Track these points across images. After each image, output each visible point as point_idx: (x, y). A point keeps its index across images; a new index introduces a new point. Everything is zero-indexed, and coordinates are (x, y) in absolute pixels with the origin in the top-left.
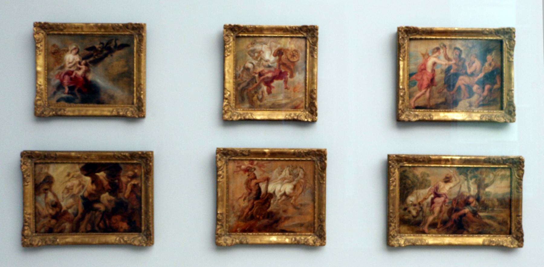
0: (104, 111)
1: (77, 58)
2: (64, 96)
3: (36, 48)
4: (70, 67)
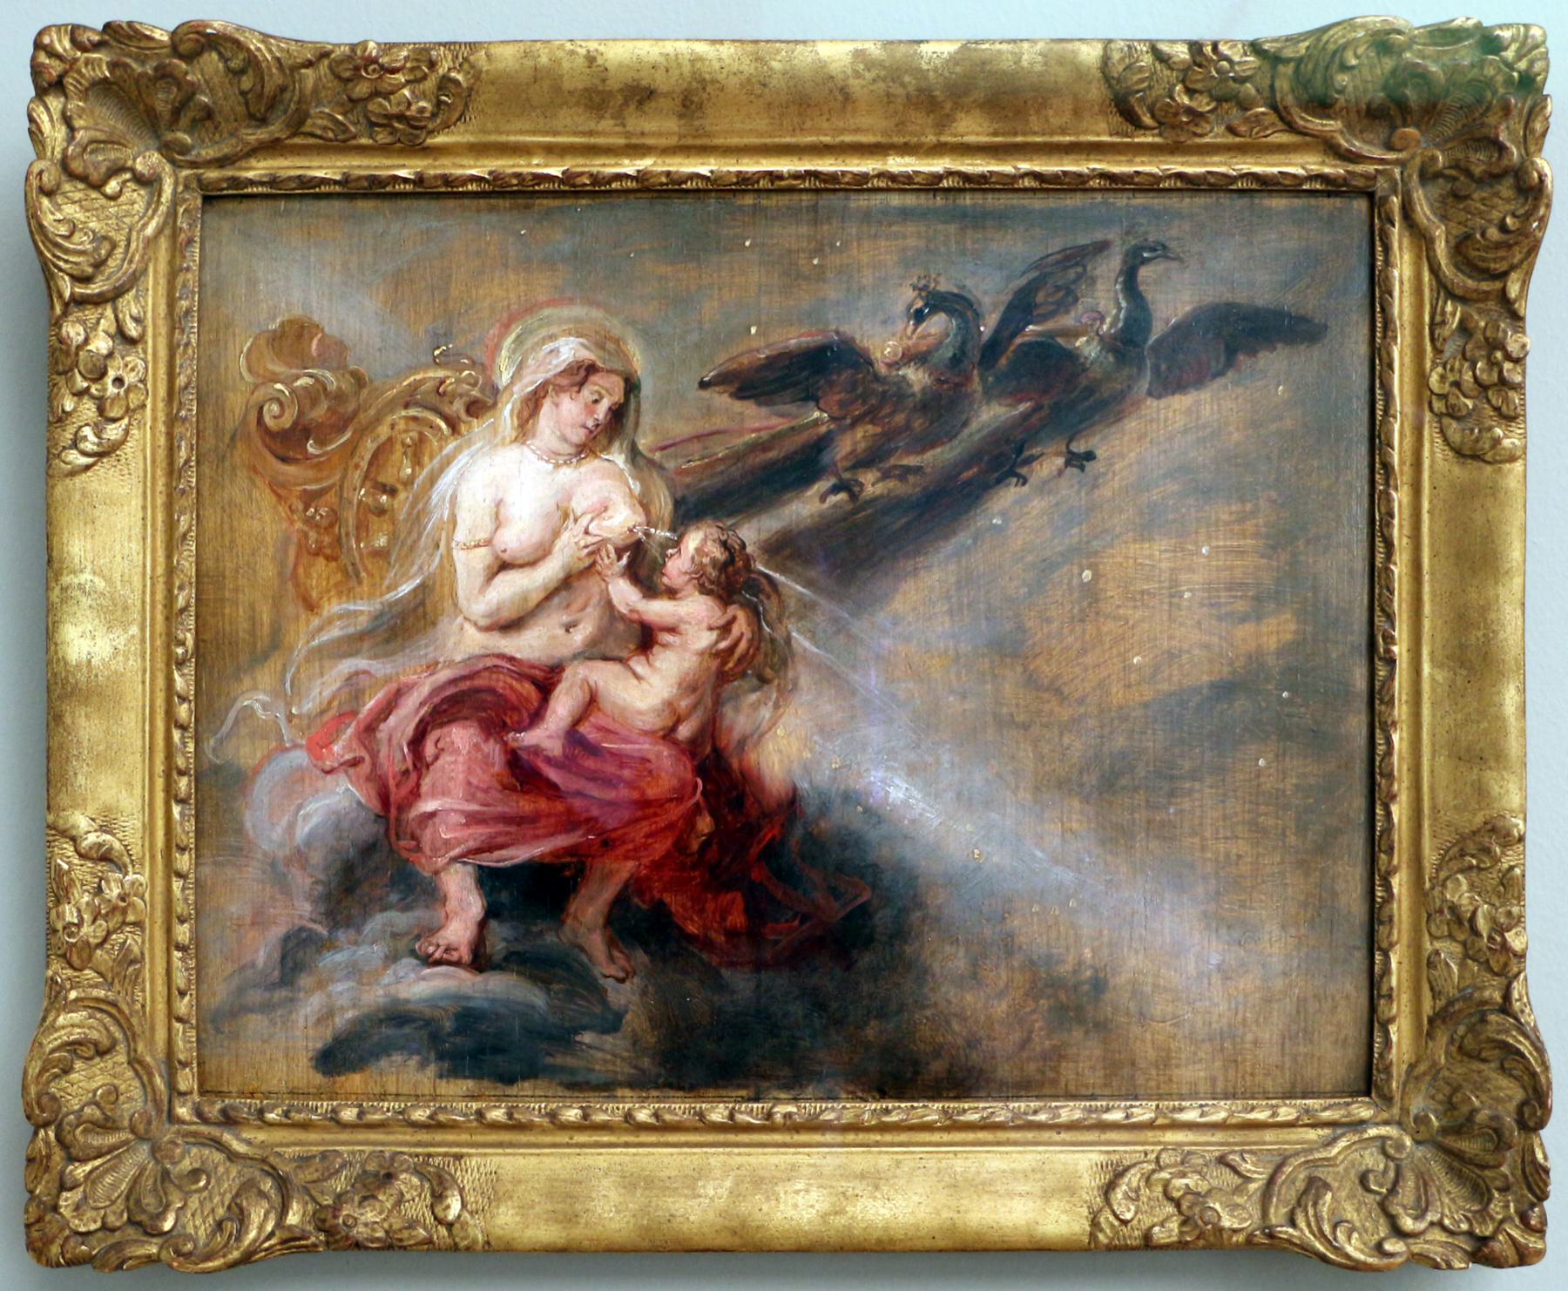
0: (983, 1186)
1: (610, 500)
2: (421, 986)
3: (60, 361)
4: (511, 625)
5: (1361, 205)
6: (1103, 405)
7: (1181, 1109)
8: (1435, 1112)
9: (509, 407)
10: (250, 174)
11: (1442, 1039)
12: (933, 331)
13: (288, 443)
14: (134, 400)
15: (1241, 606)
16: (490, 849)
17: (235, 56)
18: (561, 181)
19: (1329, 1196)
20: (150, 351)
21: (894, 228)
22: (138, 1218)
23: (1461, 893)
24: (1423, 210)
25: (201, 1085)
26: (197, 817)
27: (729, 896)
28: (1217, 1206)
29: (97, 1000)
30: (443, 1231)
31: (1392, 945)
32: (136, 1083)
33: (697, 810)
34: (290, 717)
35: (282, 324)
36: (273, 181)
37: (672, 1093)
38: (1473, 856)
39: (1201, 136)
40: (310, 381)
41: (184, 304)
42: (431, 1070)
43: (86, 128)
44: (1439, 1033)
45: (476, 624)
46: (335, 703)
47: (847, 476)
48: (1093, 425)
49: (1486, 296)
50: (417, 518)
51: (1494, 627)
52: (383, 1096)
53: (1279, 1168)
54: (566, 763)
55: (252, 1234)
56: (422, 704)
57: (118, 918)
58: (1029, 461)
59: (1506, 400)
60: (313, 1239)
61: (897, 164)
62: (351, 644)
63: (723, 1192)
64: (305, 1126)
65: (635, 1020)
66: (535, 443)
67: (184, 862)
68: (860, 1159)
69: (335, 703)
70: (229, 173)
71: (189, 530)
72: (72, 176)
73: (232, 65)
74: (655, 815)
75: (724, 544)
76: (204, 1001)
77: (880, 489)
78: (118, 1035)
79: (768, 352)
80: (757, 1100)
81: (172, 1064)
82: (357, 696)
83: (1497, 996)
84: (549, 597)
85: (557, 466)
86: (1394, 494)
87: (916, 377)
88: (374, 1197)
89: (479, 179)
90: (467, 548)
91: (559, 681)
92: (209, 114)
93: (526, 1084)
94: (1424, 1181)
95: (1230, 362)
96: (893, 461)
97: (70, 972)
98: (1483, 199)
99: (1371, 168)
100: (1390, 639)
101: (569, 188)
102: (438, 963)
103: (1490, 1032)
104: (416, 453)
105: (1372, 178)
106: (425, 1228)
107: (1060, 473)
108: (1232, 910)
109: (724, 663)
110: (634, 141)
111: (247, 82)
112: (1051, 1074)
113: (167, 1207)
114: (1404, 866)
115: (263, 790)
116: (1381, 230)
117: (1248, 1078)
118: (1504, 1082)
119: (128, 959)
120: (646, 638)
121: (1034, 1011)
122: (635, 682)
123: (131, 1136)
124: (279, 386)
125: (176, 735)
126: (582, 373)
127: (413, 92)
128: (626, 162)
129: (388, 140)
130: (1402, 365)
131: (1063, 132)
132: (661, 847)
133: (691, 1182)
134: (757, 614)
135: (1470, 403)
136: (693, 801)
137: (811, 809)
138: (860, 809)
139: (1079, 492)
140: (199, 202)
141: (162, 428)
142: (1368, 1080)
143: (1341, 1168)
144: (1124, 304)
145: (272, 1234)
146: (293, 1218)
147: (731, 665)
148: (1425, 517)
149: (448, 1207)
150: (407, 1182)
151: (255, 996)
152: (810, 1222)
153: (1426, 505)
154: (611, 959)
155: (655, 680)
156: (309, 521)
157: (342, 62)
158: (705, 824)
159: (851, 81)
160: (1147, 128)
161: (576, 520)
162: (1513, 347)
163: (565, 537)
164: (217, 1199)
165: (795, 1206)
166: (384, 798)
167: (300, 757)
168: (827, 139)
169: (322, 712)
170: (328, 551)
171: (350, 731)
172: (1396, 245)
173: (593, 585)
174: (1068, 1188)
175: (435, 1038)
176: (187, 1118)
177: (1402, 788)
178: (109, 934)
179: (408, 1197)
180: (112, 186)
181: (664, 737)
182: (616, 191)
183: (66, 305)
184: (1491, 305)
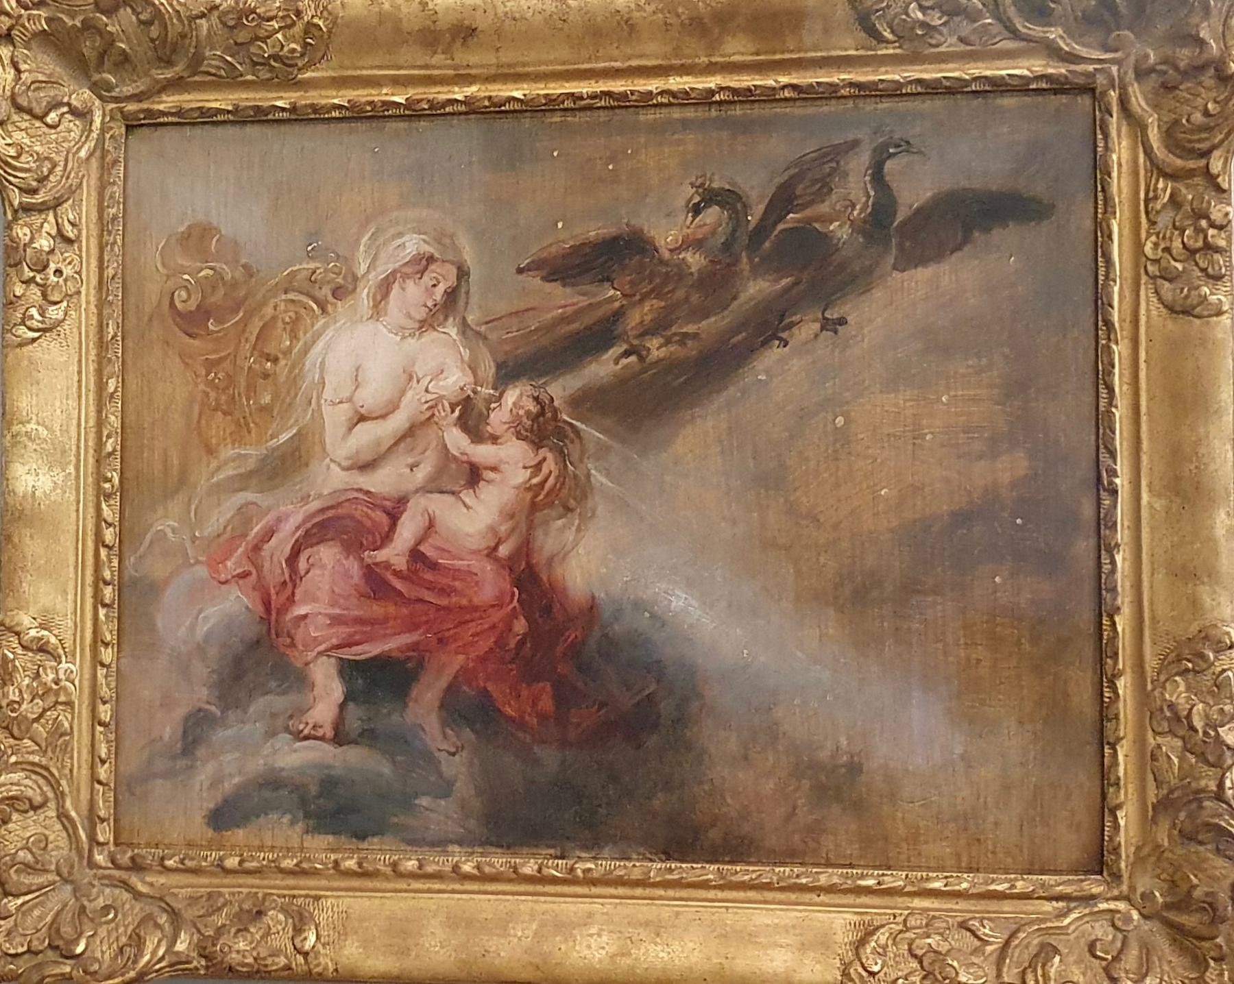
0: (750, 937)
1: (446, 364)
2: (293, 757)
5: (1085, 101)
6: (854, 279)
7: (928, 879)
8: (1160, 890)
9: (366, 291)
10: (161, 107)
11: (1164, 825)
12: (708, 221)
13: (192, 321)
14: (71, 288)
15: (977, 446)
16: (350, 645)
17: (144, 9)
18: (406, 107)
19: (1057, 959)
20: (84, 249)
21: (676, 136)
22: (56, 943)
23: (1178, 693)
24: (1139, 100)
25: (115, 839)
26: (119, 619)
27: (541, 685)
28: (955, 964)
29: (33, 764)
30: (300, 959)
31: (1119, 739)
32: (64, 834)
33: (514, 614)
34: (194, 539)
35: (190, 227)
36: (179, 113)
37: (493, 850)
38: (1189, 661)
39: (937, 46)
40: (211, 272)
41: (113, 211)
42: (299, 827)
43: (30, 71)
44: (1161, 818)
45: (339, 465)
46: (229, 528)
47: (636, 342)
48: (844, 296)
49: (1190, 173)
50: (294, 380)
51: (1205, 460)
52: (261, 848)
53: (1013, 935)
54: (407, 576)
55: (147, 958)
56: (298, 528)
57: (51, 699)
58: (790, 326)
59: (1212, 263)
60: (195, 963)
61: (676, 83)
62: (242, 482)
63: (529, 933)
64: (196, 871)
65: (464, 788)
66: (385, 320)
67: (107, 655)
68: (644, 910)
69: (229, 528)
70: (145, 106)
71: (116, 391)
72: (20, 109)
73: (142, 17)
74: (481, 618)
75: (536, 399)
76: (122, 768)
77: (662, 353)
78: (50, 795)
79: (572, 243)
80: (562, 857)
81: (93, 819)
82: (247, 522)
83: (1213, 786)
84: (396, 444)
85: (404, 338)
86: (1114, 347)
87: (694, 260)
88: (246, 930)
89: (340, 107)
90: (333, 404)
91: (405, 510)
92: (125, 58)
93: (376, 840)
94: (1147, 950)
95: (966, 240)
96: (674, 329)
97: (11, 741)
98: (1188, 89)
99: (1091, 68)
100: (1113, 473)
101: (412, 113)
102: (306, 738)
103: (1205, 817)
104: (293, 328)
105: (1091, 75)
106: (286, 957)
107: (816, 336)
108: (973, 707)
109: (536, 496)
110: (462, 72)
111: (154, 31)
112: (812, 845)
113: (80, 935)
114: (1128, 670)
115: (171, 596)
116: (1102, 120)
117: (990, 855)
118: (1220, 862)
119: (58, 732)
120: (474, 475)
121: (797, 789)
122: (465, 510)
123: (58, 878)
124: (186, 277)
125: (103, 552)
126: (424, 262)
127: (285, 36)
128: (456, 89)
129: (268, 75)
130: (1120, 236)
131: (816, 49)
132: (485, 644)
133: (503, 925)
134: (562, 452)
135: (1179, 266)
136: (511, 607)
137: (606, 614)
138: (647, 615)
139: (833, 351)
140: (123, 130)
141: (93, 309)
142: (1099, 860)
143: (1072, 937)
144: (872, 193)
145: (163, 958)
146: (181, 946)
147: (541, 497)
148: (1143, 366)
149: (305, 939)
150: (275, 917)
151: (161, 765)
152: (600, 961)
153: (1143, 355)
154: (445, 736)
155: (481, 509)
156: (210, 383)
157: (228, 12)
158: (520, 626)
159: (637, 14)
160: (888, 42)
161: (418, 382)
162: (1216, 215)
163: (409, 394)
164: (121, 930)
165: (589, 947)
166: (267, 604)
167: (202, 571)
168: (617, 64)
169: (219, 536)
170: (224, 407)
171: (240, 550)
172: (1114, 133)
173: (431, 432)
174: (823, 943)
175: (303, 801)
176: (103, 864)
177: (1124, 601)
178: (45, 711)
179: (274, 930)
180: (52, 117)
181: (488, 556)
182: (449, 114)
183: (15, 211)
184: (1197, 180)
